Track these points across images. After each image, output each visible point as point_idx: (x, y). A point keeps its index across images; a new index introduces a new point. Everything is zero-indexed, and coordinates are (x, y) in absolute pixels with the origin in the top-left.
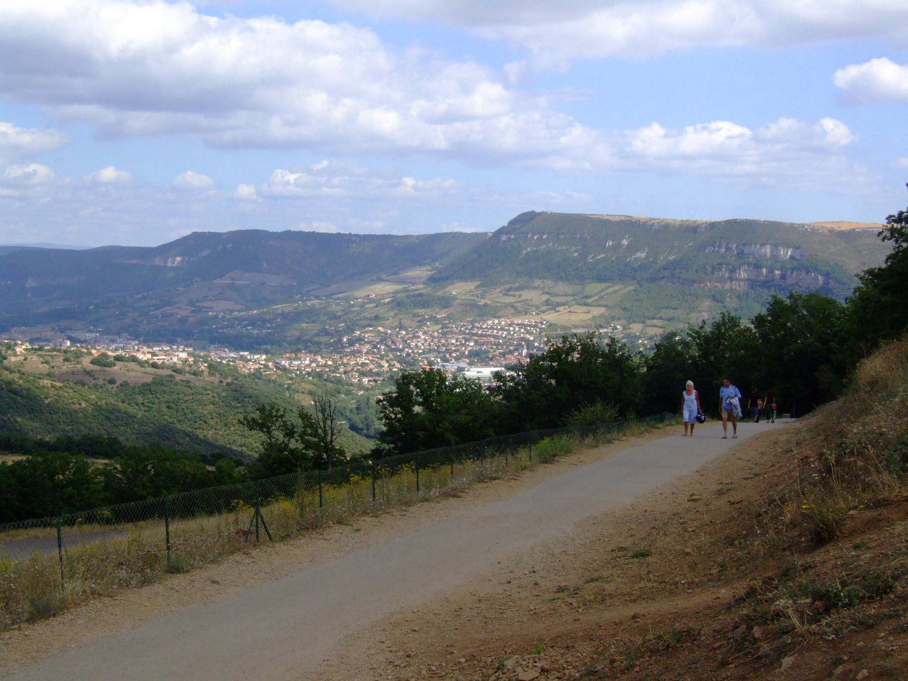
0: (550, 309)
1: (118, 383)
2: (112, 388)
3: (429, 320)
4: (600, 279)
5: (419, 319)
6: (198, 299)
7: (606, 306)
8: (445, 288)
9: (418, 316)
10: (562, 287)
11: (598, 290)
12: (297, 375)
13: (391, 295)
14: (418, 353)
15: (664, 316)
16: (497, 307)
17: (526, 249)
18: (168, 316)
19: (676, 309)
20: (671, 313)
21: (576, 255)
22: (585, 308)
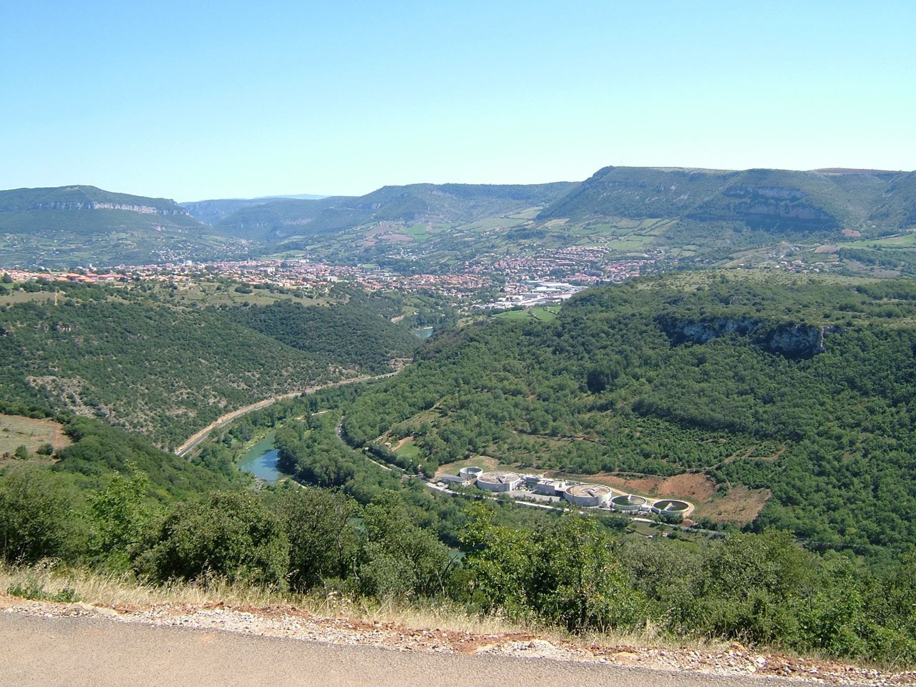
3: (528, 247)
4: (652, 216)
10: (625, 222)
20: (702, 241)
22: (640, 238)
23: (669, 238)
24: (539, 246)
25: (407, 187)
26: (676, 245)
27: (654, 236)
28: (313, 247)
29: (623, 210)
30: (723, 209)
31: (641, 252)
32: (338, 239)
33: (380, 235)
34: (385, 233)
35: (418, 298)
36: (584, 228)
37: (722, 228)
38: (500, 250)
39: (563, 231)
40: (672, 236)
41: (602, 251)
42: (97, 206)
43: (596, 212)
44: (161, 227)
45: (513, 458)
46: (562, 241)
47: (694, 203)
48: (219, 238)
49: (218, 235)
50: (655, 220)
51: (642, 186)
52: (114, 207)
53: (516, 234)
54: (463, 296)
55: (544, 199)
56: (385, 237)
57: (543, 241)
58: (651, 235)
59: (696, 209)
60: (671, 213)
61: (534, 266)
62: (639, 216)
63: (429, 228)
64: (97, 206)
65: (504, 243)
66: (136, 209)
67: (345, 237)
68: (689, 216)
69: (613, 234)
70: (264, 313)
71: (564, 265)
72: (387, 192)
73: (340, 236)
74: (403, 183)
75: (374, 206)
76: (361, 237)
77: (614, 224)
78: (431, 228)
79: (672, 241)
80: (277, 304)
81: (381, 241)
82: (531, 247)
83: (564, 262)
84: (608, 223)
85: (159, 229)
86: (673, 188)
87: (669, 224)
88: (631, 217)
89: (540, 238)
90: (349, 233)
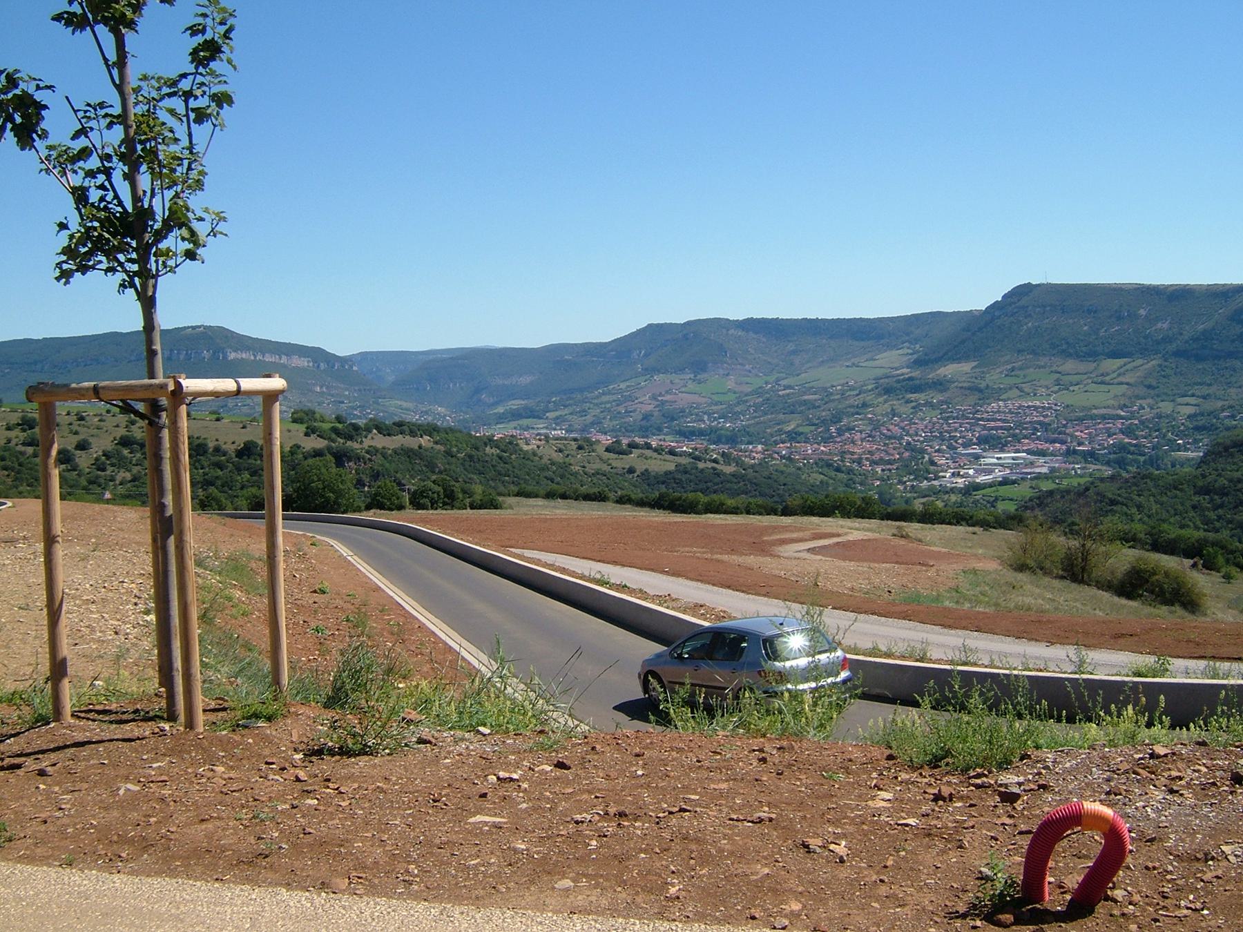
0: (1064, 389)
1: (638, 473)
2: (633, 478)
3: (925, 405)
4: (1115, 355)
5: (914, 404)
6: (661, 393)
7: (1127, 384)
8: (936, 370)
9: (912, 401)
10: (1070, 365)
11: (1115, 367)
12: (804, 464)
13: (874, 382)
14: (918, 441)
15: (1198, 393)
16: (1001, 389)
17: (1026, 324)
18: (631, 412)
19: (1210, 385)
20: (1205, 390)
21: (1086, 328)
22: (1103, 388)
23: (1149, 387)
24: (942, 402)
25: (689, 323)
26: (1164, 397)
27: (1127, 384)
28: (557, 413)
29: (1064, 347)
30: (1233, 341)
31: (1113, 407)
32: (596, 401)
33: (660, 395)
34: (667, 392)
35: (821, 473)
36: (1006, 376)
37: (1234, 370)
38: (879, 410)
39: (974, 380)
40: (1154, 383)
41: (1051, 408)
42: (232, 356)
43: (1019, 351)
44: (321, 387)
45: (22, 835)
46: (978, 395)
47: (1181, 334)
48: (405, 404)
49: (401, 400)
50: (1119, 362)
51: (1089, 311)
52: (255, 357)
53: (899, 385)
54: (883, 470)
55: (907, 338)
56: (668, 397)
57: (947, 395)
58: (1122, 383)
59: (1187, 342)
60: (1146, 350)
61: (946, 431)
62: (1092, 355)
63: (730, 384)
64: (232, 356)
65: (881, 400)
66: (284, 360)
67: (605, 398)
68: (1178, 354)
69: (1057, 382)
70: (663, 483)
71: (996, 428)
72: (655, 333)
73: (597, 397)
74: (681, 319)
75: (635, 354)
76: (631, 399)
77: (1054, 368)
78: (734, 385)
79: (1156, 391)
80: (682, 468)
81: (663, 403)
82: (929, 404)
83: (992, 424)
84: (1043, 367)
85: (318, 389)
86: (1142, 312)
87: (1146, 366)
88: (1079, 356)
89: (941, 391)
90: (609, 393)
